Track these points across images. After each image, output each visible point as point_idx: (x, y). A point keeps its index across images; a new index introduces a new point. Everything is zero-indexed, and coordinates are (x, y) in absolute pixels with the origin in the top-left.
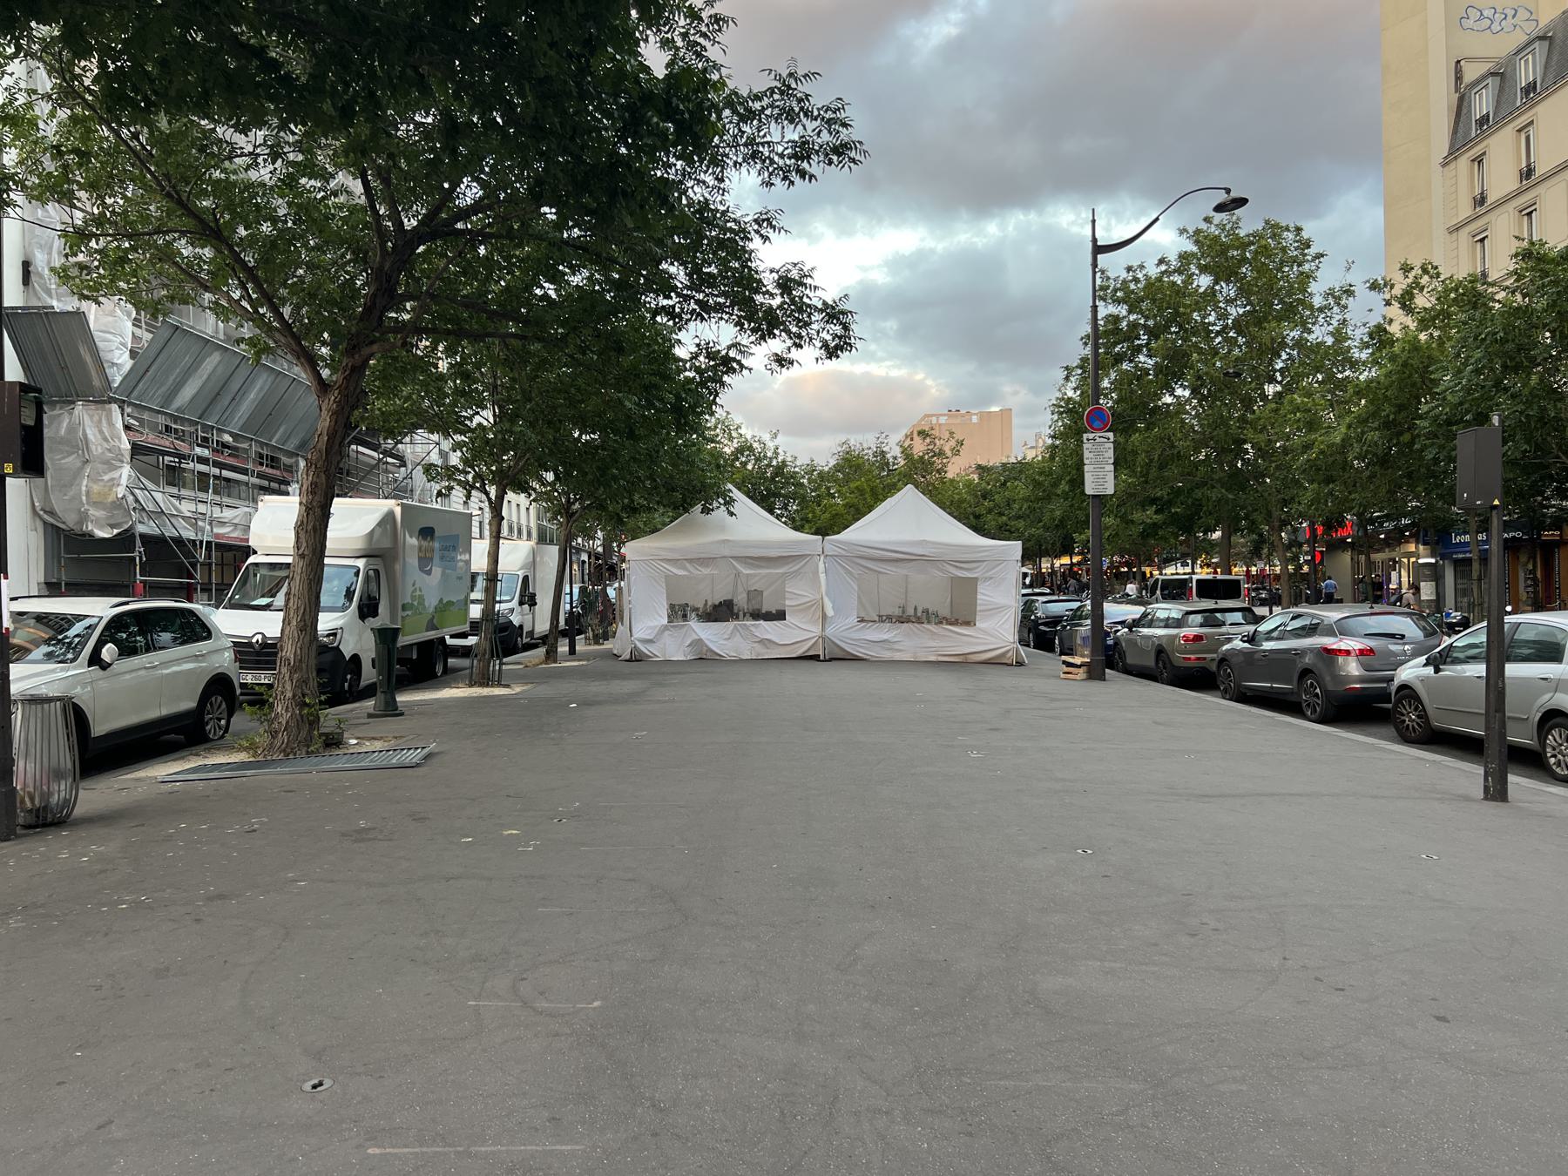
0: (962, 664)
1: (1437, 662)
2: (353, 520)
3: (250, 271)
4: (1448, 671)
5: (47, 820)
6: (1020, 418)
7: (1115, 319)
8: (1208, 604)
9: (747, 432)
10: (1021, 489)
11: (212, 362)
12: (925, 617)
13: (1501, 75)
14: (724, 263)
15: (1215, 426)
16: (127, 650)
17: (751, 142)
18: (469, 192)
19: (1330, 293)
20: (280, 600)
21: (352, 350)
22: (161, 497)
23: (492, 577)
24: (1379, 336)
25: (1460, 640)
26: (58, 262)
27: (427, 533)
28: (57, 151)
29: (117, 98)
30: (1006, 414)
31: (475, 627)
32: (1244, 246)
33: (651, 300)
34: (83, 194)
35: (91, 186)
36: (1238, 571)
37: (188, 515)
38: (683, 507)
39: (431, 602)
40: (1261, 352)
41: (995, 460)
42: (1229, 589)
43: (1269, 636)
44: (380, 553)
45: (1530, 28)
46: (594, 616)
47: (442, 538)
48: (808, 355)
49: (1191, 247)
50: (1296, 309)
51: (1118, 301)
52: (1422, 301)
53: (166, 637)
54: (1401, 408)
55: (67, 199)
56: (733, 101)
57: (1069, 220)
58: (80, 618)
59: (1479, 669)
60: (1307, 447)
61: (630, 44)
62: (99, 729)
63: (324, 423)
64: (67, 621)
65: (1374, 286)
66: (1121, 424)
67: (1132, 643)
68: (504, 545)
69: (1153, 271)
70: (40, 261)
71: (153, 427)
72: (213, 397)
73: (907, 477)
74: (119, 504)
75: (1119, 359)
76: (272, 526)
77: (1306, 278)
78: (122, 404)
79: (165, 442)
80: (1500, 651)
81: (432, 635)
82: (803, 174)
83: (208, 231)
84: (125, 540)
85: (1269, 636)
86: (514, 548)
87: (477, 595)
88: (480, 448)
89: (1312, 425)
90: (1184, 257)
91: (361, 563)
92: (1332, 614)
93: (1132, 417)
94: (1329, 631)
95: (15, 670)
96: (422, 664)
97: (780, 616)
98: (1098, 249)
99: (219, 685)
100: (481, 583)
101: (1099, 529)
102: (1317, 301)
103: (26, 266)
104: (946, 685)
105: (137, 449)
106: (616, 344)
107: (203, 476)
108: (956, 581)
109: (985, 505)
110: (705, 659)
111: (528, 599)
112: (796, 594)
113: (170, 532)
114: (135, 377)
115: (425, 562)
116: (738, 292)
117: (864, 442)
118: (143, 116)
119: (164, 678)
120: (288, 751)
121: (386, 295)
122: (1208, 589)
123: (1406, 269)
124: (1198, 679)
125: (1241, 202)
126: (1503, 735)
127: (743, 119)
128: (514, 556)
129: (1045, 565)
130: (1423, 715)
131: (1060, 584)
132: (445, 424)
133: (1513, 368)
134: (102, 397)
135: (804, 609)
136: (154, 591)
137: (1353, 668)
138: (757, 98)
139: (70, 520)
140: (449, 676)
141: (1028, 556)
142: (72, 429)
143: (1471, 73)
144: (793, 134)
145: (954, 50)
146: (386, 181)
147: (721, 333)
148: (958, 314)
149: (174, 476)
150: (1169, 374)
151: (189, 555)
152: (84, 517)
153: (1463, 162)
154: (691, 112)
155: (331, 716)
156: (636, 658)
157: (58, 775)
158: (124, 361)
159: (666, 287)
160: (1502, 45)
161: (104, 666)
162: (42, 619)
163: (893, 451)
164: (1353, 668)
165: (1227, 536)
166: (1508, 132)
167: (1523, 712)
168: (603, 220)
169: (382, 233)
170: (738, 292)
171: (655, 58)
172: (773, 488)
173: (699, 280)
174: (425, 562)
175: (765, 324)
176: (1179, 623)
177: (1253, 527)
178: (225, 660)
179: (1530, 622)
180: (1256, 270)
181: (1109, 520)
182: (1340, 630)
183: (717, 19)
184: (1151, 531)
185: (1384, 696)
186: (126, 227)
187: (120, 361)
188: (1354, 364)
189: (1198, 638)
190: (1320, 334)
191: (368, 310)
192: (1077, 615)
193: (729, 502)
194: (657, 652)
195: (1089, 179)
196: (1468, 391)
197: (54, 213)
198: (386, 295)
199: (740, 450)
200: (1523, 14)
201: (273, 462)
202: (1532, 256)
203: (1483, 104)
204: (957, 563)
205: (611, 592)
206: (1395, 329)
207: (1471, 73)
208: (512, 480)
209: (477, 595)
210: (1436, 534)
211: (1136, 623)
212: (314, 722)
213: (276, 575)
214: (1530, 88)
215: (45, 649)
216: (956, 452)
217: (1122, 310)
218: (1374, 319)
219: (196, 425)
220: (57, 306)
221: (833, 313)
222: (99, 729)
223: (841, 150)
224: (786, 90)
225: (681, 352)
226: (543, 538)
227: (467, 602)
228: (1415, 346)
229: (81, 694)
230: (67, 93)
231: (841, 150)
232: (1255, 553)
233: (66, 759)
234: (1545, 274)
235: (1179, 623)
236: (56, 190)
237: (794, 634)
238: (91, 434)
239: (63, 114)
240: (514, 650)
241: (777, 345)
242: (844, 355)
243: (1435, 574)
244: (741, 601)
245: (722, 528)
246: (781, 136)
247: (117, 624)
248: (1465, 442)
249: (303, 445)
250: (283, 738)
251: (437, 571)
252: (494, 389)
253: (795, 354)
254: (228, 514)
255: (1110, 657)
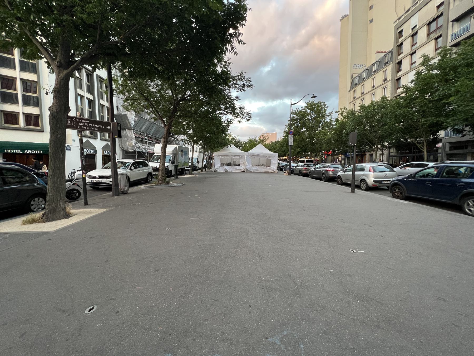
0: (268, 173)
1: (344, 172)
2: (170, 148)
3: (154, 106)
4: (346, 173)
5: (124, 193)
6: (278, 135)
7: (294, 117)
8: (308, 163)
9: (233, 136)
10: (278, 145)
11: (147, 123)
12: (263, 165)
13: (359, 76)
14: (230, 105)
15: (310, 135)
16: (135, 168)
17: (235, 84)
18: (189, 93)
19: (330, 113)
20: (159, 161)
21: (170, 119)
22: (140, 145)
23: (192, 158)
24: (337, 120)
25: (348, 168)
26: (122, 104)
27: (182, 151)
28: (122, 85)
29: (132, 76)
30: (276, 133)
31: (190, 166)
32: (315, 105)
33: (218, 112)
34: (126, 93)
35: (127, 92)
36: (313, 159)
37: (144, 148)
38: (224, 147)
39: (183, 162)
40: (318, 123)
41: (274, 141)
42: (312, 161)
43: (317, 168)
44: (175, 154)
45: (365, 68)
46: (208, 165)
47: (184, 151)
48: (244, 120)
49: (306, 105)
50: (323, 116)
51: (294, 114)
52: (344, 114)
53: (142, 166)
54: (340, 132)
55: (124, 94)
56: (232, 77)
57: (287, 101)
58: (128, 162)
59: (351, 173)
60: (325, 138)
61: (215, 65)
62: (131, 180)
63: (166, 131)
64: (126, 163)
65: (336, 112)
66: (295, 135)
67: (295, 169)
68: (194, 153)
69: (300, 109)
70: (119, 106)
71: (138, 134)
72: (148, 129)
73: (259, 143)
74: (133, 146)
75: (294, 124)
76: (157, 149)
77: (325, 111)
78: (133, 130)
79: (140, 136)
80: (354, 170)
81: (183, 167)
82: (243, 90)
83: (147, 99)
84: (134, 152)
85: (317, 168)
86: (196, 153)
87: (190, 161)
88: (190, 137)
89: (325, 135)
90: (306, 107)
91: (172, 155)
92: (328, 164)
93: (297, 133)
94: (327, 167)
95: (118, 170)
96: (182, 172)
97: (239, 165)
98: (292, 104)
99: (150, 174)
100: (191, 159)
101: (291, 152)
102: (327, 114)
103: (117, 107)
104: (266, 175)
105: (136, 137)
106: (213, 119)
107: (146, 142)
108: (267, 159)
109: (272, 147)
110: (227, 172)
111: (198, 162)
112: (242, 161)
113: (141, 151)
114: (135, 125)
115: (182, 155)
116: (233, 110)
117: (253, 138)
118: (135, 79)
119: (141, 173)
120: (161, 184)
121: (175, 110)
122: (307, 161)
123: (341, 109)
124: (306, 175)
125: (315, 97)
126: (354, 183)
127: (234, 80)
128: (196, 155)
129: (282, 158)
130: (342, 180)
131: (285, 161)
132: (185, 133)
133: (359, 125)
134: (130, 129)
135: (242, 164)
136: (138, 159)
137: (331, 173)
138: (236, 77)
139: (126, 149)
140: (186, 174)
141: (279, 156)
142: (125, 134)
143: (354, 76)
144: (242, 83)
145: (269, 72)
146: (175, 91)
147: (230, 117)
148: (269, 117)
149: (142, 142)
150: (302, 127)
151: (144, 154)
152: (128, 148)
153: (352, 91)
154: (225, 78)
155: (167, 179)
156: (215, 171)
157: (126, 186)
158: (133, 123)
159: (220, 109)
160: (360, 71)
161: (132, 170)
162: (122, 163)
163: (257, 139)
164: (331, 173)
165: (311, 153)
166: (360, 86)
167: (358, 179)
168: (210, 96)
169: (175, 100)
170: (233, 110)
171: (219, 69)
172: (238, 144)
173: (226, 108)
174: (182, 155)
175: (237, 115)
176: (303, 166)
177: (315, 152)
178: (151, 170)
179: (359, 165)
180: (317, 109)
181: (292, 151)
182: (329, 167)
183: (229, 63)
184: (299, 152)
185: (335, 178)
186: (134, 100)
187: (133, 123)
188: (333, 125)
189: (306, 169)
190: (328, 120)
191: (172, 112)
192: (287, 165)
193: (231, 145)
194: (219, 170)
195: (291, 95)
196: (351, 129)
197: (121, 96)
198: (175, 110)
199: (232, 139)
200: (364, 66)
201: (157, 140)
202: (362, 107)
203: (356, 81)
204: (268, 156)
205: (211, 162)
206: (340, 119)
207: (354, 76)
208: (196, 142)
209: (190, 161)
210: (345, 153)
211: (296, 166)
212: (165, 179)
213: (158, 158)
214: (364, 78)
215: (122, 168)
216: (268, 139)
217: (295, 116)
218: (336, 117)
219: (145, 134)
220: (123, 114)
221: (248, 114)
222: (131, 180)
223: (250, 86)
224: (241, 75)
225: (223, 120)
226: (200, 152)
227: (188, 162)
228: (343, 122)
229: (129, 174)
230: (123, 75)
231: (250, 86)
232: (316, 156)
233: (127, 184)
234: (365, 110)
235: (303, 166)
236: (122, 92)
237: (241, 168)
238: (129, 135)
239: (122, 79)
240: (196, 170)
241: (239, 119)
242: (250, 121)
243: (344, 159)
244: (232, 163)
245: (229, 150)
246: (240, 83)
247: (133, 164)
248: (351, 135)
249: (162, 137)
250: (160, 182)
251: (184, 157)
252: (192, 127)
253: (242, 120)
254: (150, 148)
255: (292, 172)
